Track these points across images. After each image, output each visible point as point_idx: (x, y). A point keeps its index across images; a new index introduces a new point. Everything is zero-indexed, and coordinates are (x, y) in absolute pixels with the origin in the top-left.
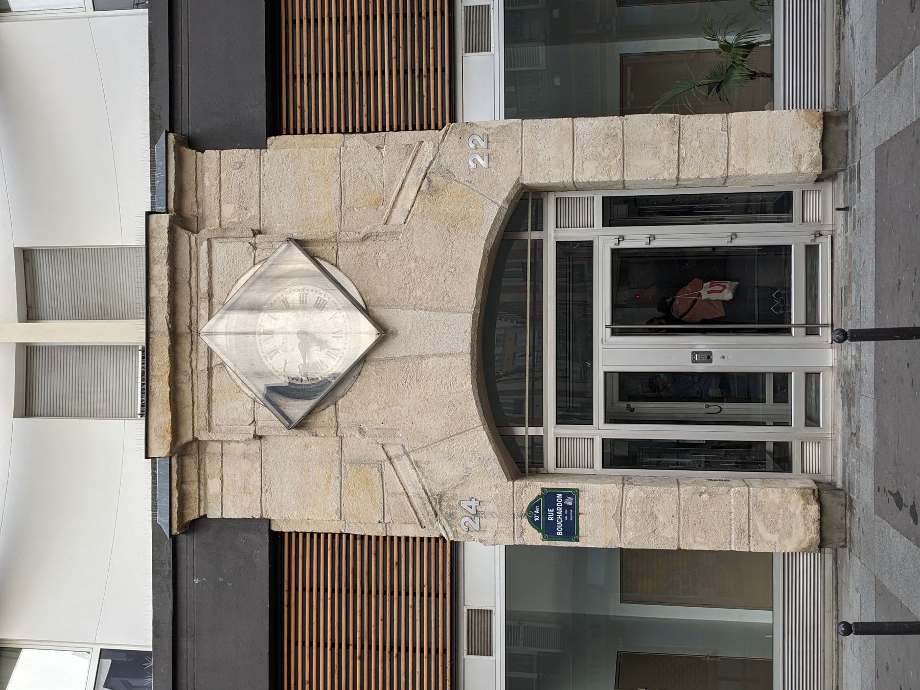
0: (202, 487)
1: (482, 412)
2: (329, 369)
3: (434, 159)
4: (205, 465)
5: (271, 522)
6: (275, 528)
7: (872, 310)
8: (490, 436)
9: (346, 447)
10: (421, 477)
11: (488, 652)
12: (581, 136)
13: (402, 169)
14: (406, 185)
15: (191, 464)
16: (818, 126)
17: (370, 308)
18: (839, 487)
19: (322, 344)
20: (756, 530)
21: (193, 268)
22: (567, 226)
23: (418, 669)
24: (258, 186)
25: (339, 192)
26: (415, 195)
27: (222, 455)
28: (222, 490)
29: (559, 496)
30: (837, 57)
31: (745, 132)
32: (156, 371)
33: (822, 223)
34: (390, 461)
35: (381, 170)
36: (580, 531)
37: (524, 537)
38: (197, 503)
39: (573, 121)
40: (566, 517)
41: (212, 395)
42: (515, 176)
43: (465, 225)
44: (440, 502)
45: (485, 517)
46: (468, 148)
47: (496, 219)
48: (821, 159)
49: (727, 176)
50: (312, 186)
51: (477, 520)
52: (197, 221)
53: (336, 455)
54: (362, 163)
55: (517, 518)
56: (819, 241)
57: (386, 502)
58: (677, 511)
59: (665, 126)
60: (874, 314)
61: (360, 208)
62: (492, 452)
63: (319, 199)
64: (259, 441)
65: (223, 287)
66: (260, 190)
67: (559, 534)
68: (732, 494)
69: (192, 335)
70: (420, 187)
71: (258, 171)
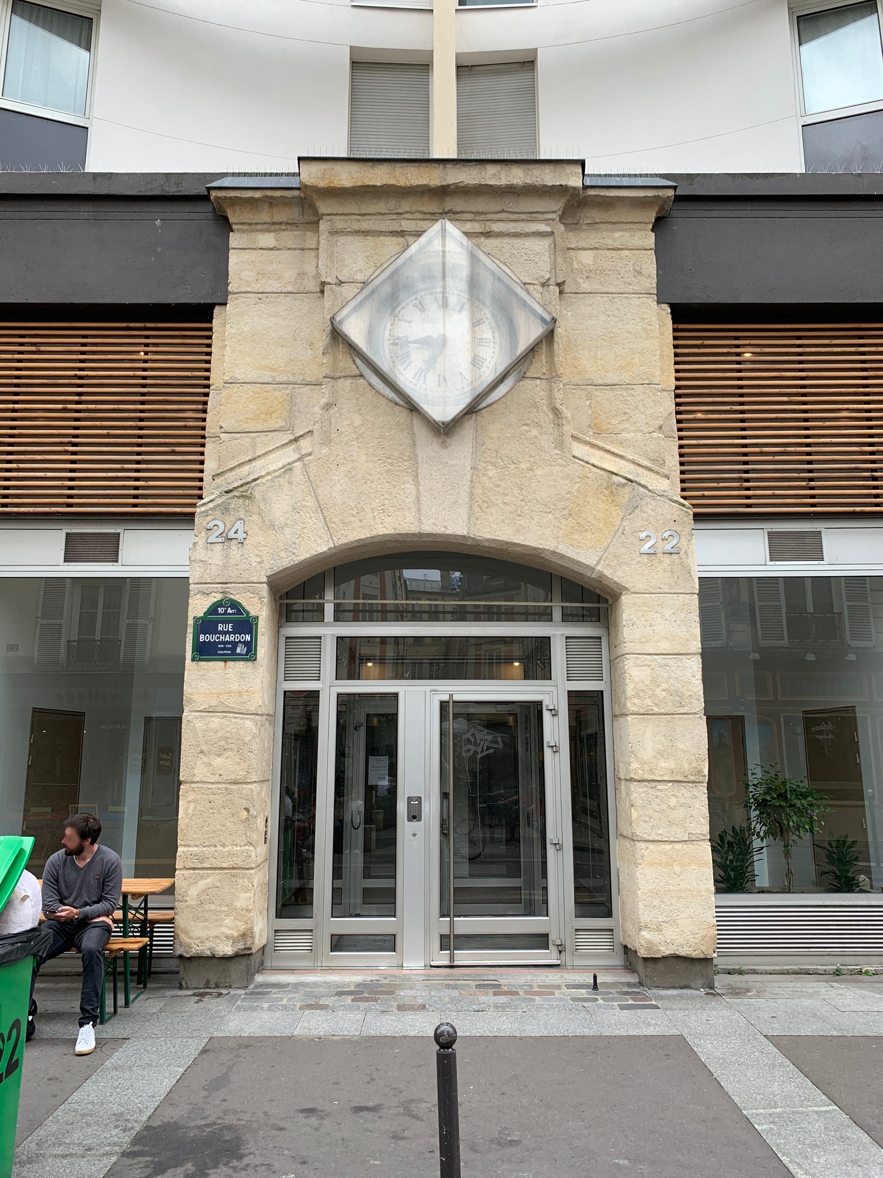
0: (266, 226)
1: (351, 546)
2: (402, 371)
3: (649, 491)
4: (291, 230)
5: (224, 306)
6: (217, 310)
7: (473, 1031)
8: (321, 556)
9: (311, 390)
10: (273, 475)
11: (69, 557)
12: (679, 664)
13: (636, 455)
14: (617, 460)
15: (293, 213)
16: (696, 952)
17: (474, 416)
18: (256, 977)
19: (431, 363)
20: (203, 877)
21: (520, 215)
22: (568, 650)
23: (49, 474)
24: (614, 290)
25: (608, 382)
26: (607, 468)
27: (303, 250)
28: (262, 249)
29: (248, 638)
30: (774, 970)
31: (689, 861)
32: (401, 170)
33: (575, 953)
34: (293, 440)
35: (635, 431)
36: (205, 663)
37: (198, 596)
38: (247, 221)
39: (697, 654)
40: (223, 646)
41: (372, 236)
42: (631, 585)
43: (572, 527)
44: (242, 496)
45: (224, 550)
46: (664, 530)
47: (579, 563)
48: (656, 956)
49: (634, 841)
50: (615, 352)
51: (220, 540)
52: (573, 224)
53: (301, 377)
54: (642, 409)
55: (221, 587)
56: (553, 949)
57: (244, 435)
58: (227, 780)
59: (694, 764)
60: (469, 1034)
61: (591, 406)
62: (302, 558)
63: (601, 360)
64: (318, 290)
65: (498, 248)
66: (610, 293)
67: (202, 638)
68: (246, 847)
69: (442, 214)
70: (616, 474)
71: (631, 291)
